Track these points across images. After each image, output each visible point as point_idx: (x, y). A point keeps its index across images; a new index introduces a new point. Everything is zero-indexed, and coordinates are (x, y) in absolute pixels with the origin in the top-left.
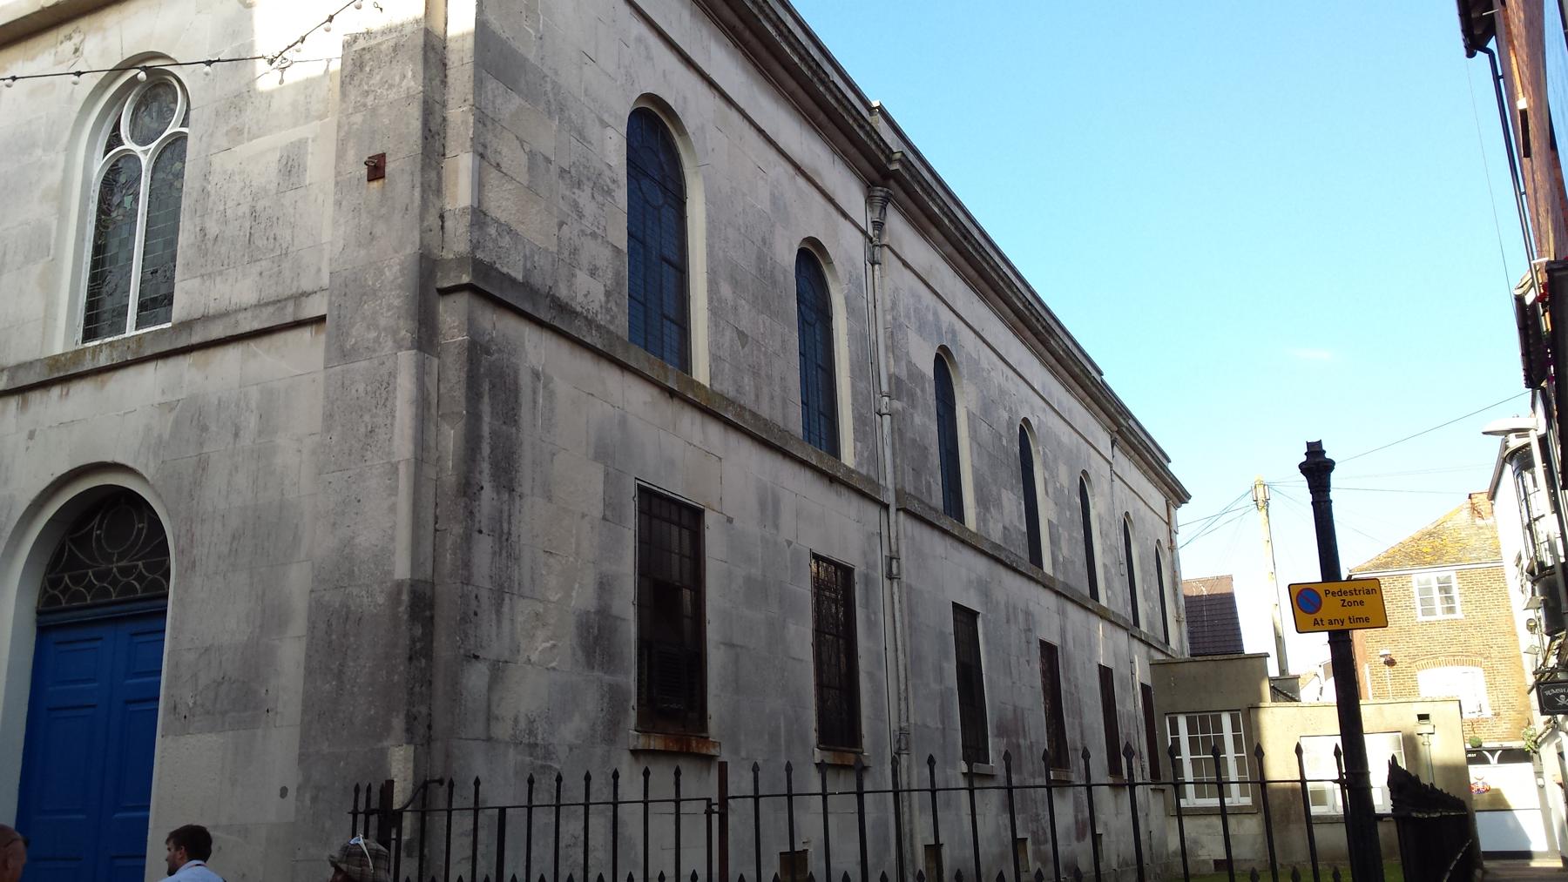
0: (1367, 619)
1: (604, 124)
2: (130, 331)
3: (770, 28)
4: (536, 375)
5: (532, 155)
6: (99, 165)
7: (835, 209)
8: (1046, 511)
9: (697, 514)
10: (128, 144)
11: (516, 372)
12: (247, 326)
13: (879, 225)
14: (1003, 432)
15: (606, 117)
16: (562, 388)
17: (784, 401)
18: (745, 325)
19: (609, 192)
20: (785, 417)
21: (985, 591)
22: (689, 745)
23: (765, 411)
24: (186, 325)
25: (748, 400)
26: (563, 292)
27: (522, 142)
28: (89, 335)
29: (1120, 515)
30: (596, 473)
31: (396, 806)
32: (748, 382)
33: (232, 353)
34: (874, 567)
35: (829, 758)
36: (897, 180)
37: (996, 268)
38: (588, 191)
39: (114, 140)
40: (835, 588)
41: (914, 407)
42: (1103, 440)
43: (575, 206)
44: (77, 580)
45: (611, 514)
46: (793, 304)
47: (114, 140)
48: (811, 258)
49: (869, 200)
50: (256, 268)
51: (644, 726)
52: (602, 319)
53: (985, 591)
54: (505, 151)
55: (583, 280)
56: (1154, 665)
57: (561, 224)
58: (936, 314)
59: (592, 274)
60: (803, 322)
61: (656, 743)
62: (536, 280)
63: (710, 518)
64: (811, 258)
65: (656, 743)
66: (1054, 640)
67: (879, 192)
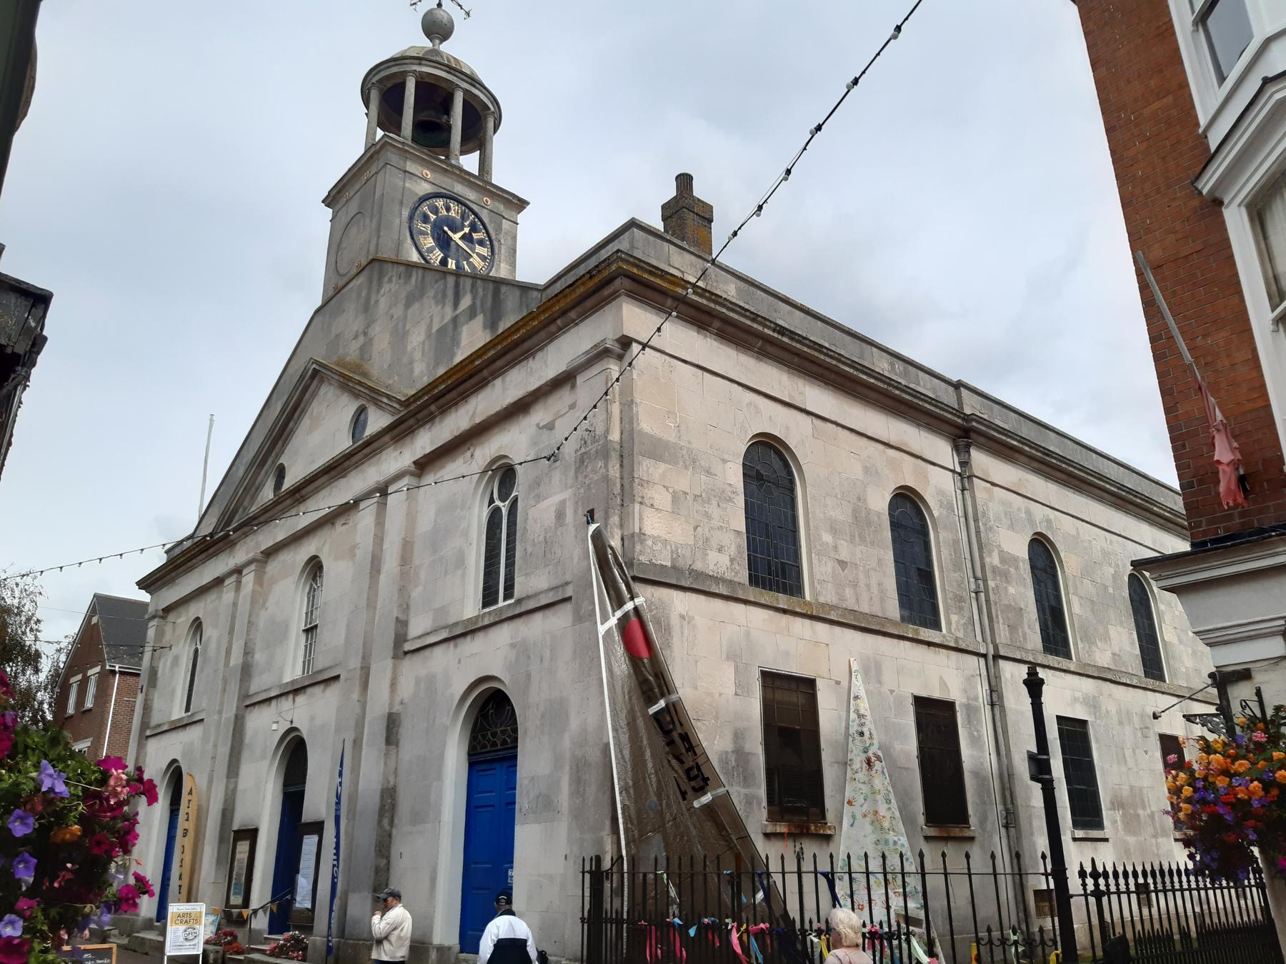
1: (725, 461)
3: (847, 369)
4: (682, 617)
6: (486, 512)
7: (931, 465)
9: (810, 683)
10: (498, 503)
11: (668, 618)
12: (544, 601)
14: (1109, 583)
15: (726, 457)
16: (699, 621)
17: (882, 600)
18: (844, 555)
19: (730, 500)
20: (883, 610)
21: (1093, 704)
22: (808, 829)
23: (865, 608)
25: (850, 603)
26: (698, 566)
27: (667, 488)
28: (485, 605)
30: (729, 671)
32: (848, 592)
33: (538, 617)
34: (976, 699)
35: (932, 832)
36: (971, 428)
38: (714, 502)
39: (491, 501)
41: (1008, 582)
43: (708, 516)
44: (484, 737)
45: (741, 689)
46: (888, 534)
47: (491, 501)
49: (956, 448)
50: (547, 570)
51: (772, 818)
52: (728, 576)
54: (656, 496)
55: (713, 556)
57: (695, 528)
58: (1028, 512)
59: (720, 551)
61: (781, 828)
62: (680, 563)
63: (819, 684)
65: (781, 828)
67: (962, 442)
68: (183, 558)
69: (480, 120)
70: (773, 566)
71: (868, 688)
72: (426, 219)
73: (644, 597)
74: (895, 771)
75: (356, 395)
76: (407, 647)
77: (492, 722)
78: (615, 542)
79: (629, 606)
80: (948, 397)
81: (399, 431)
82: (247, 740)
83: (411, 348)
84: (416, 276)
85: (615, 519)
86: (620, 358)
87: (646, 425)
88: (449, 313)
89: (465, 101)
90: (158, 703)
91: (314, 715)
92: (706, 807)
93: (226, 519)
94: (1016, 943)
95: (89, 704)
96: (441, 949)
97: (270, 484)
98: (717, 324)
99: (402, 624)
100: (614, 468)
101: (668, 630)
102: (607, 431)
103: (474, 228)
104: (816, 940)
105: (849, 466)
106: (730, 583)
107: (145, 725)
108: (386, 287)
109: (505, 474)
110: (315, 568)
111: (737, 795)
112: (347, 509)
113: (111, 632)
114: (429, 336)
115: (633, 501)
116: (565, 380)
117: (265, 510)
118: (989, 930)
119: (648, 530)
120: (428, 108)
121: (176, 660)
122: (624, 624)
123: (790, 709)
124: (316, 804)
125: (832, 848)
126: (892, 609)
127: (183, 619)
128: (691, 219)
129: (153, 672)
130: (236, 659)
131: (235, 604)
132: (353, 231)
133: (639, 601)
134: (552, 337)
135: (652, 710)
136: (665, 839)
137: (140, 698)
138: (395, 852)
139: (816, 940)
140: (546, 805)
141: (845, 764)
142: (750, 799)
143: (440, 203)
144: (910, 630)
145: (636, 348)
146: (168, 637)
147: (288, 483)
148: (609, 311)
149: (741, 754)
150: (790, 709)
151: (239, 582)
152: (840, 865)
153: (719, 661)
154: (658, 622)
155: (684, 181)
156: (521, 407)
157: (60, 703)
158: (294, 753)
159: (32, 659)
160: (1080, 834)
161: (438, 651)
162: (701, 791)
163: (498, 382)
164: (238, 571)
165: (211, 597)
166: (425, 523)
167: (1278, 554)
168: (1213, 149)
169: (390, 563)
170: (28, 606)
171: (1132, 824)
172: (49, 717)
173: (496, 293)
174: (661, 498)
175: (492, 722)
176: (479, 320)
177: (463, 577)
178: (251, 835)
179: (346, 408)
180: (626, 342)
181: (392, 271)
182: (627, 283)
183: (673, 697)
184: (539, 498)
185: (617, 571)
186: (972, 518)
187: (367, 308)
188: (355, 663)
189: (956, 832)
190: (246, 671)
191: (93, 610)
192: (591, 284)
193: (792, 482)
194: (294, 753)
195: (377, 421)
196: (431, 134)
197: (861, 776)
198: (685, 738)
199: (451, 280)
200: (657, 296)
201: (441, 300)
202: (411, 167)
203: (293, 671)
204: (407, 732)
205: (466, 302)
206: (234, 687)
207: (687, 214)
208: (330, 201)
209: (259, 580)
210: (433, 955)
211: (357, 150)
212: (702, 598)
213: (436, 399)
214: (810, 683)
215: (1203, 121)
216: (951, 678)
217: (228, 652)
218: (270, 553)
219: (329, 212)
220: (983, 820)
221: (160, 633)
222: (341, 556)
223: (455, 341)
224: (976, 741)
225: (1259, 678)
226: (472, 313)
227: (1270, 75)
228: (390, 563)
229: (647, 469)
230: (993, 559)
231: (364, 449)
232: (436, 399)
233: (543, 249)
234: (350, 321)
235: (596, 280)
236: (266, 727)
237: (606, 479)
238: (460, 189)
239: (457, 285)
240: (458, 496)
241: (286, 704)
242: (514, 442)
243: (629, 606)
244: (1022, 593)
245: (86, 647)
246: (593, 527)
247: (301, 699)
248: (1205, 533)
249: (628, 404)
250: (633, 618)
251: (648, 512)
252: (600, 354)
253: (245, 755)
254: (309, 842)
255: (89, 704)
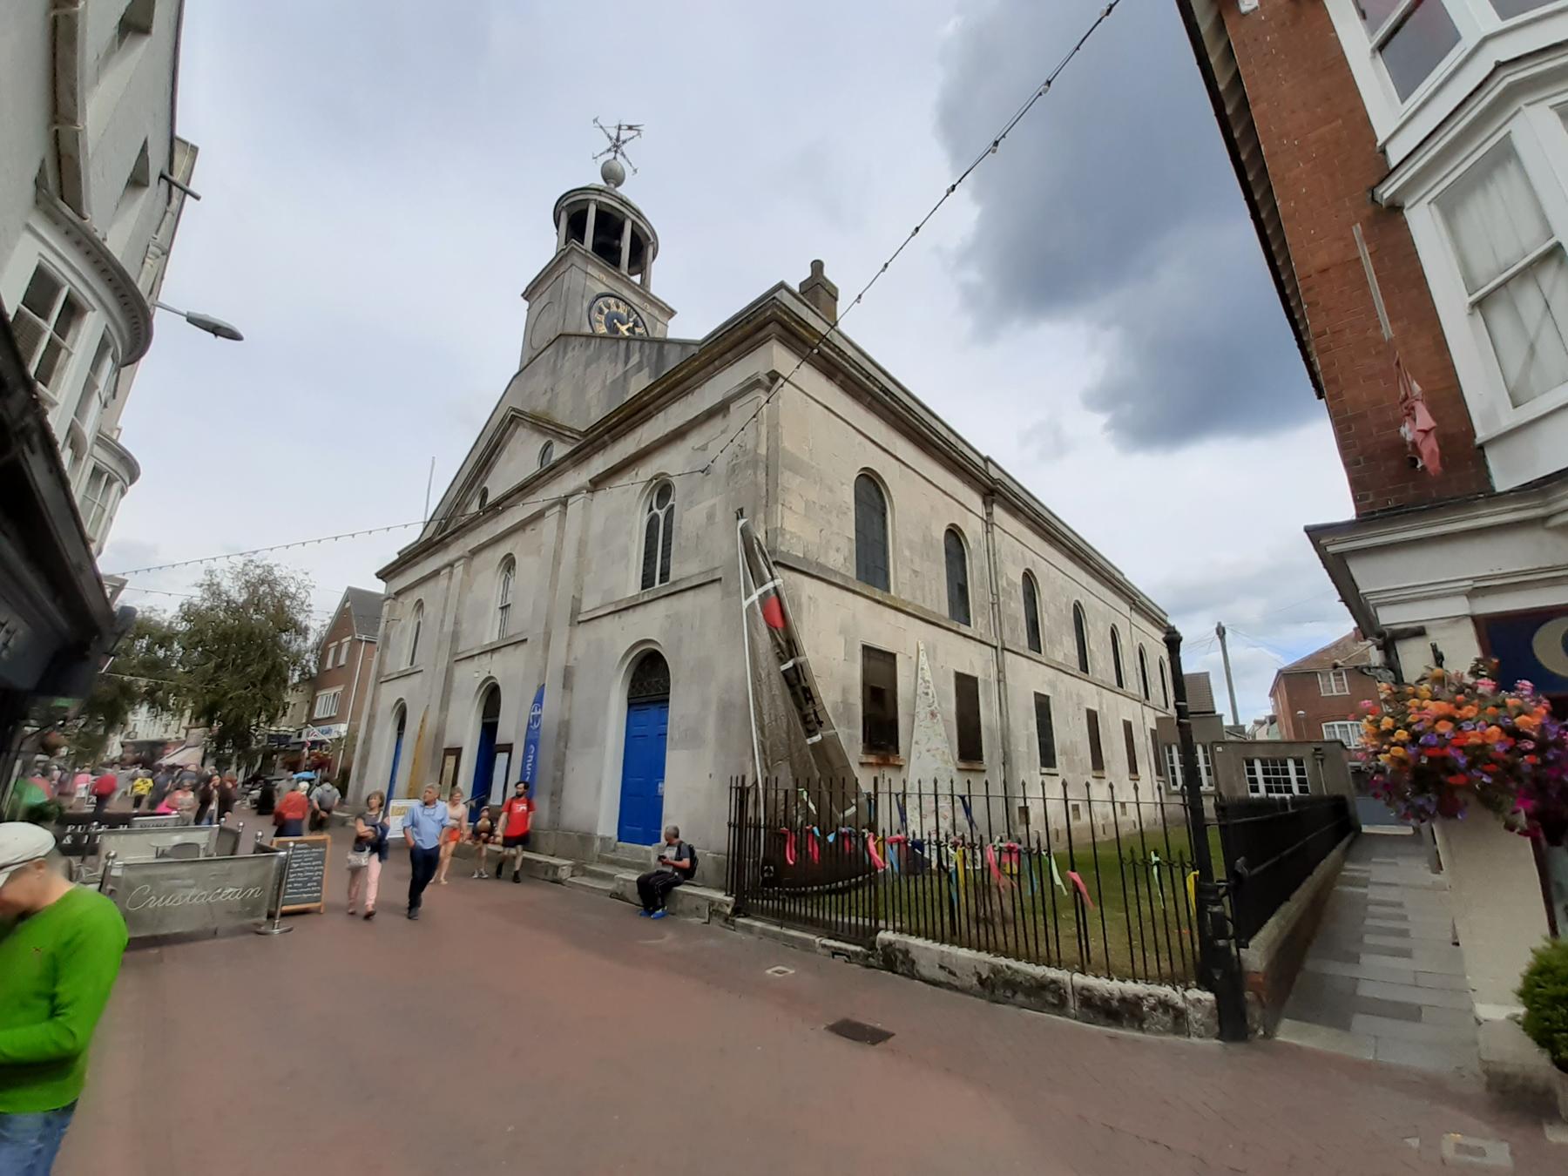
0: (834, 954)
2: (657, 585)
5: (807, 502)
6: (646, 518)
7: (967, 509)
8: (1091, 645)
9: (893, 656)
13: (989, 514)
21: (1053, 686)
23: (928, 606)
24: (674, 583)
25: (919, 602)
26: (822, 560)
28: (643, 588)
29: (1136, 645)
31: (1478, 441)
33: (690, 594)
35: (962, 765)
36: (996, 491)
37: (1056, 529)
40: (966, 687)
42: (1125, 608)
43: (829, 522)
45: (848, 657)
47: (651, 509)
48: (954, 533)
49: (984, 503)
53: (1053, 686)
55: (832, 553)
56: (1158, 720)
60: (949, 563)
62: (809, 556)
63: (899, 657)
64: (954, 533)
65: (872, 759)
66: (1095, 708)
67: (989, 499)
68: (409, 558)
69: (642, 248)
70: (872, 565)
71: (929, 665)
72: (601, 312)
73: (782, 579)
74: (945, 721)
75: (545, 434)
76: (581, 618)
77: (649, 676)
78: (761, 536)
79: (770, 585)
80: (981, 463)
81: (579, 456)
82: (455, 685)
83: (587, 396)
84: (594, 343)
85: (761, 516)
86: (768, 390)
87: (787, 444)
88: (620, 369)
89: (633, 232)
90: (388, 659)
91: (508, 669)
92: (813, 745)
93: (442, 528)
94: (1157, 863)
95: (342, 662)
96: (603, 839)
97: (477, 502)
98: (841, 377)
99: (577, 602)
100: (763, 475)
101: (799, 607)
102: (757, 446)
103: (636, 325)
104: (951, 851)
105: (923, 503)
106: (843, 576)
107: (379, 674)
108: (570, 354)
109: (663, 490)
110: (509, 563)
111: (842, 733)
112: (539, 516)
113: (357, 613)
114: (604, 387)
115: (776, 501)
116: (721, 409)
117: (472, 520)
118: (1181, 854)
119: (787, 526)
120: (602, 230)
121: (403, 631)
122: (764, 598)
123: (879, 675)
124: (510, 729)
125: (902, 775)
126: (944, 610)
127: (410, 600)
128: (823, 295)
129: (387, 638)
130: (448, 627)
131: (448, 588)
132: (544, 317)
133: (778, 582)
134: (709, 377)
135: (784, 667)
136: (792, 765)
137: (376, 655)
138: (568, 767)
139: (951, 851)
140: (693, 739)
141: (913, 717)
142: (849, 735)
143: (612, 301)
144: (954, 625)
145: (781, 381)
146: (397, 615)
147: (490, 500)
148: (761, 351)
149: (847, 705)
150: (879, 675)
151: (451, 573)
152: (912, 788)
153: (835, 633)
154: (792, 600)
155: (817, 266)
156: (679, 434)
157: (322, 661)
158: (491, 696)
159: (303, 631)
160: (1045, 770)
161: (605, 620)
162: (810, 733)
163: (661, 415)
164: (451, 565)
165: (430, 585)
166: (596, 527)
167: (1477, 517)
168: (1394, 162)
169: (569, 555)
170: (303, 595)
171: (1071, 764)
172: (314, 671)
173: (661, 350)
174: (798, 505)
175: (649, 676)
176: (646, 371)
177: (627, 568)
178: (457, 752)
179: (538, 442)
180: (774, 376)
181: (576, 342)
182: (778, 328)
183: (801, 659)
184: (691, 504)
185: (759, 557)
186: (991, 552)
187: (554, 371)
188: (540, 629)
189: (976, 766)
190: (455, 637)
191: (346, 600)
192: (748, 327)
193: (885, 508)
194: (491, 696)
195: (560, 450)
196: (606, 251)
197: (928, 722)
198: (807, 691)
199: (623, 344)
200: (799, 344)
201: (614, 359)
202: (590, 269)
203: (491, 636)
204: (579, 681)
205: (635, 359)
206: (446, 646)
207: (818, 288)
208: (527, 295)
209: (467, 571)
210: (598, 843)
211: (549, 254)
212: (824, 585)
213: (609, 430)
214: (893, 656)
215: (1381, 137)
216: (975, 661)
217: (442, 621)
218: (475, 552)
219: (526, 304)
220: (991, 757)
221: (392, 610)
222: (530, 553)
223: (625, 389)
224: (989, 704)
225: (1434, 636)
226: (639, 367)
227: (1503, 59)
228: (569, 555)
229: (787, 479)
230: (1003, 583)
231: (550, 472)
232: (609, 430)
233: (693, 322)
234: (540, 381)
235: (752, 325)
236: (470, 677)
237: (756, 485)
238: (626, 293)
239: (628, 347)
240: (626, 505)
241: (486, 659)
242: (671, 463)
243: (770, 585)
244: (1017, 607)
245: (342, 623)
246: (742, 522)
247: (496, 656)
248: (1372, 504)
249: (774, 427)
250: (773, 595)
251: (787, 513)
252: (754, 385)
253: (454, 696)
254: (501, 759)
255: (342, 662)
